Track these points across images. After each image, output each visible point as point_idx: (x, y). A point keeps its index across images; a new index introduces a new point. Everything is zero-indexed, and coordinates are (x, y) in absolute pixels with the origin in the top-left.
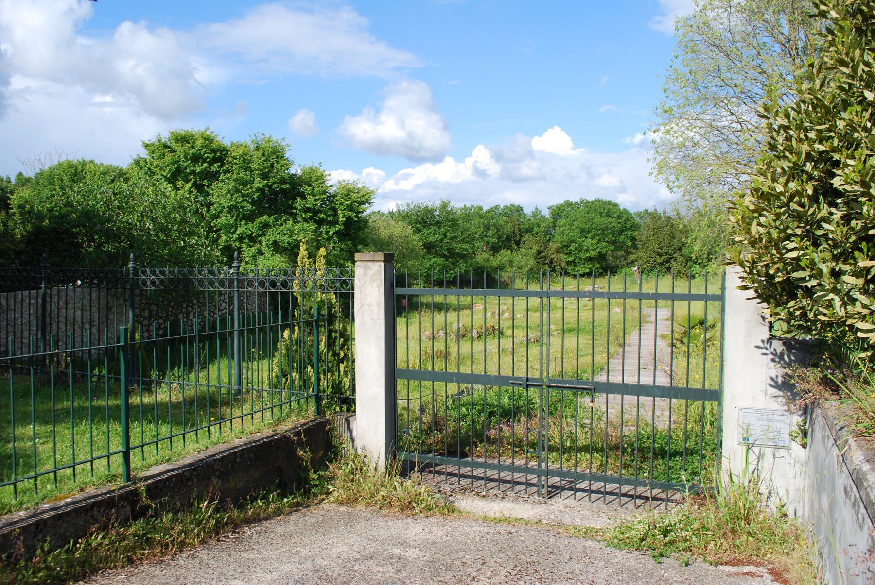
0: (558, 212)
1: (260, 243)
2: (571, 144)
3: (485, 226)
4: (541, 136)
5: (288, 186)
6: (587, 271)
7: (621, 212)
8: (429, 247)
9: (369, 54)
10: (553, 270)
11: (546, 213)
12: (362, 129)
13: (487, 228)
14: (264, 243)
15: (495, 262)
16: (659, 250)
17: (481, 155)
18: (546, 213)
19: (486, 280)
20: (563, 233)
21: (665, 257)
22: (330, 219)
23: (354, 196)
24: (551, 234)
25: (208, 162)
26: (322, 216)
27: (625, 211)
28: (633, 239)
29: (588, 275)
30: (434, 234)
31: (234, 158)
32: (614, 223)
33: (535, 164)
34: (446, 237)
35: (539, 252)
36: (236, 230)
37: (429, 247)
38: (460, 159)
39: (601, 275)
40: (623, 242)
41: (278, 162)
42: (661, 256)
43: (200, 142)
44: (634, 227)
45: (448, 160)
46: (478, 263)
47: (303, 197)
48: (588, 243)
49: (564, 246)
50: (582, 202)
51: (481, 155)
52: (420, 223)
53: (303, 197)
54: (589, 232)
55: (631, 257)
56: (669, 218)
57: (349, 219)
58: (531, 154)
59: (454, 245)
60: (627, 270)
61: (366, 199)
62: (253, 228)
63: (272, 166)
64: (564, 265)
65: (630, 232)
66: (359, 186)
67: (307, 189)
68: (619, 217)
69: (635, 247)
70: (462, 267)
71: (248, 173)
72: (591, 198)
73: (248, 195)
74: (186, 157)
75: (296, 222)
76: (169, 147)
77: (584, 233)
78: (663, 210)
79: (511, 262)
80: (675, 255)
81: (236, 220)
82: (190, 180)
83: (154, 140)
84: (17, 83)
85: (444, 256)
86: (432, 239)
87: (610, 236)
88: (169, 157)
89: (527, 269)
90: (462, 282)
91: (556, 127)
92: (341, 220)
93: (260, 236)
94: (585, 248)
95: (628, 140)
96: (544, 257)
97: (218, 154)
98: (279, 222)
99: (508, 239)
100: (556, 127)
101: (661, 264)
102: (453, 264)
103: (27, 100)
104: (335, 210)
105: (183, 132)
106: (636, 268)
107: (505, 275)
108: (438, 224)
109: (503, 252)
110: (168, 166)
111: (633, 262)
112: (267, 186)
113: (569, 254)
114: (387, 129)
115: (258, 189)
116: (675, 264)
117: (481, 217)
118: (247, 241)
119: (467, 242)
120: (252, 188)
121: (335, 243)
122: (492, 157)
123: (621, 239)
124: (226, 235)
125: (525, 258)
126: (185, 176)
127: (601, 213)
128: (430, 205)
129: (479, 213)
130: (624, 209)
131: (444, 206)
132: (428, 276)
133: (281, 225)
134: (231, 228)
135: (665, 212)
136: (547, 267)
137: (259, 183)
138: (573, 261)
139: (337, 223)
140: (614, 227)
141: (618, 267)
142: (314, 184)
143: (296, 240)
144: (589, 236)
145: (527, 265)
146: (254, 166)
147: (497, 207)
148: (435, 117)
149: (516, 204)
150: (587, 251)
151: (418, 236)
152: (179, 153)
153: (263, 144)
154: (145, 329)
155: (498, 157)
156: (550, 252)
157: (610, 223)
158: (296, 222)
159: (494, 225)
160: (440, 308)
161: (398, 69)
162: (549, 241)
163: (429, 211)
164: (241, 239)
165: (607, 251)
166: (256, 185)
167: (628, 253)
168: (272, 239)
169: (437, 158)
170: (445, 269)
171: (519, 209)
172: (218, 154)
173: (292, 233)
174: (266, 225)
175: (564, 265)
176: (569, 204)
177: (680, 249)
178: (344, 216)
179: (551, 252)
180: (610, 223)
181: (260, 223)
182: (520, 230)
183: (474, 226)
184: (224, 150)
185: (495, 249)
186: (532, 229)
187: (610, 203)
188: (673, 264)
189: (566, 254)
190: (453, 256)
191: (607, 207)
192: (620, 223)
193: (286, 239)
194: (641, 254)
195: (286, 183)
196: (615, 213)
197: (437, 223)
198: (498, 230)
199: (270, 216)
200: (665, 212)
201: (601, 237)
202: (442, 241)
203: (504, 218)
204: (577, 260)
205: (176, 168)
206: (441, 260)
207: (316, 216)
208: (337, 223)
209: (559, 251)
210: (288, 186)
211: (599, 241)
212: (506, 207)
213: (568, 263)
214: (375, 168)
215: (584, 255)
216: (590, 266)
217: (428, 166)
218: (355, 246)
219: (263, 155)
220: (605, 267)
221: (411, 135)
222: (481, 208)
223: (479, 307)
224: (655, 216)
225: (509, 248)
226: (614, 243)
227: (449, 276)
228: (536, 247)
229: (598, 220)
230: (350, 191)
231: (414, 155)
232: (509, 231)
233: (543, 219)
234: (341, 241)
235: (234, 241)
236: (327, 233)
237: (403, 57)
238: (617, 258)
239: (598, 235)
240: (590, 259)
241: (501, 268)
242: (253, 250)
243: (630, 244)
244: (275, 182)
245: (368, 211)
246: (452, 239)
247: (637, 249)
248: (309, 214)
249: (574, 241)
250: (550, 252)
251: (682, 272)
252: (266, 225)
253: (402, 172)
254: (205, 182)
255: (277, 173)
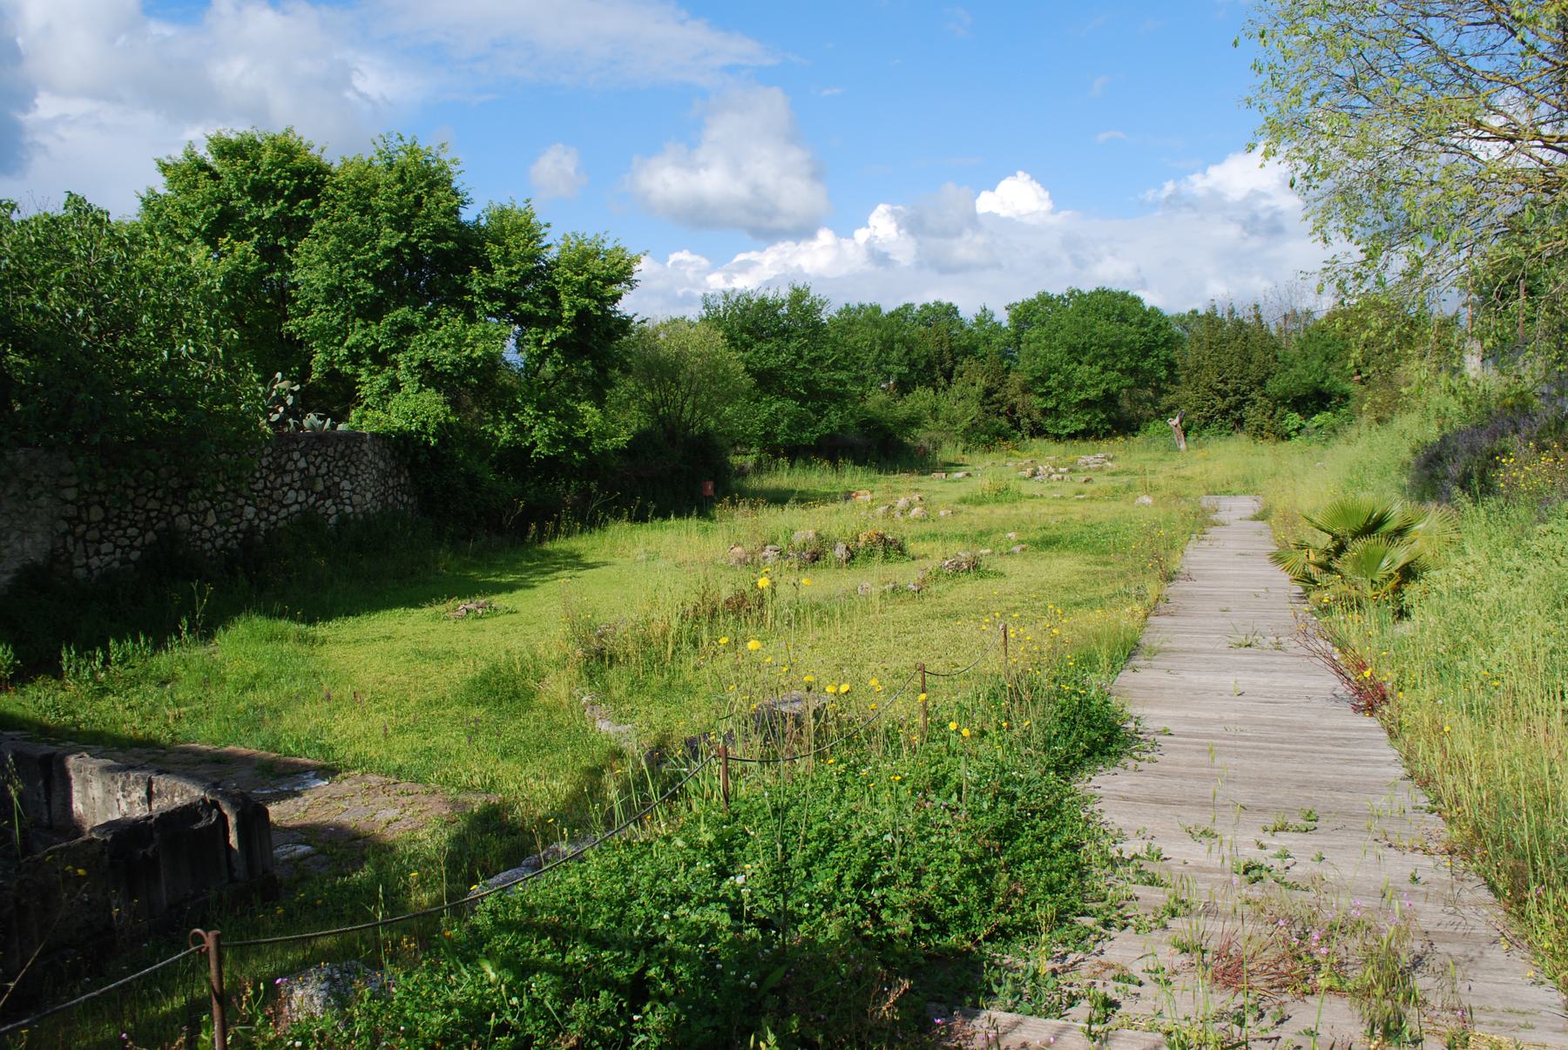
0: (1025, 315)
1: (395, 365)
2: (1047, 205)
3: (884, 343)
4: (993, 190)
5: (451, 244)
6: (1082, 426)
7: (1147, 314)
8: (767, 381)
9: (678, 44)
10: (1016, 425)
11: (1003, 318)
12: (667, 180)
13: (888, 345)
14: (402, 366)
15: (903, 409)
16: (1221, 386)
17: (882, 226)
18: (1003, 318)
19: (886, 449)
20: (1035, 354)
21: (1232, 399)
22: (543, 312)
23: (595, 265)
24: (1012, 358)
25: (287, 199)
26: (526, 306)
27: (1154, 312)
28: (1170, 365)
29: (1085, 435)
30: (778, 353)
31: (337, 187)
32: (1132, 334)
33: (979, 239)
34: (801, 357)
35: (989, 393)
36: (345, 339)
37: (767, 381)
38: (844, 230)
39: (1108, 434)
40: (1151, 371)
41: (430, 195)
42: (1224, 396)
43: (266, 157)
44: (1171, 342)
45: (825, 236)
46: (867, 412)
47: (487, 268)
48: (1082, 372)
49: (1036, 379)
50: (1071, 294)
51: (882, 226)
52: (750, 332)
53: (487, 268)
54: (1084, 351)
55: (1166, 401)
56: (1240, 325)
57: (583, 314)
58: (973, 221)
59: (818, 373)
60: (1159, 424)
61: (622, 275)
62: (379, 333)
63: (418, 202)
64: (1036, 416)
65: (1164, 351)
66: (608, 246)
67: (494, 250)
68: (1142, 324)
69: (1173, 379)
70: (833, 418)
71: (366, 218)
72: (1087, 288)
73: (365, 264)
74: (239, 188)
75: (471, 319)
76: (209, 169)
77: (1075, 353)
78: (1227, 307)
79: (935, 411)
80: (1253, 395)
81: (345, 318)
82: (252, 236)
83: (178, 155)
84: (46, 107)
85: (798, 396)
86: (772, 362)
87: (1127, 359)
88: (206, 186)
89: (965, 423)
90: (833, 450)
91: (1020, 174)
92: (566, 314)
93: (394, 350)
94: (1077, 382)
95: (1150, 195)
96: (998, 401)
97: (307, 181)
98: (435, 322)
99: (930, 366)
100: (1020, 174)
101: (1225, 413)
102: (816, 411)
103: (62, 139)
104: (554, 295)
105: (233, 137)
106: (1177, 421)
107: (921, 437)
108: (785, 333)
109: (919, 391)
110: (203, 206)
111: (1170, 409)
112: (405, 243)
113: (1047, 394)
114: (713, 181)
115: (387, 252)
116: (1252, 412)
117: (876, 324)
118: (368, 361)
119: (844, 368)
120: (373, 249)
121: (556, 364)
122: (899, 227)
123: (1147, 364)
124: (324, 350)
125: (962, 403)
126: (240, 229)
127: (1108, 316)
128: (770, 295)
129: (872, 316)
130: (1152, 308)
131: (798, 296)
132: (768, 436)
133: (437, 327)
134: (334, 336)
135: (1232, 312)
136: (1002, 426)
137: (389, 238)
138: (1055, 409)
139: (559, 321)
140: (1133, 341)
141: (1140, 418)
142: (510, 241)
143: (468, 358)
144: (1085, 359)
145: (965, 415)
146: (378, 202)
147: (908, 307)
148: (795, 156)
149: (945, 301)
150: (1081, 388)
151: (735, 355)
152: (226, 181)
153: (401, 158)
154: (91, 551)
155: (914, 225)
156: (1011, 391)
157: (1127, 333)
158: (471, 319)
159: (902, 340)
160: (779, 498)
161: (731, 70)
162: (1007, 370)
163: (766, 308)
164: (355, 358)
165: (1120, 389)
166: (383, 242)
167: (1160, 392)
168: (419, 355)
169: (804, 232)
170: (799, 424)
171: (951, 311)
172: (307, 181)
173: (460, 341)
174: (407, 329)
175: (1036, 416)
176: (1045, 300)
177: (1262, 383)
178: (573, 306)
179: (1012, 391)
180: (1127, 333)
181: (394, 323)
182: (951, 350)
183: (861, 338)
184: (319, 173)
185: (904, 387)
186: (976, 348)
187: (1124, 295)
188: (1249, 412)
189: (1041, 395)
190: (814, 395)
191: (1120, 304)
192: (1144, 334)
193: (448, 355)
194: (1185, 392)
195: (447, 238)
196: (1135, 315)
197: (785, 330)
198: (910, 350)
199: (415, 309)
200: (1232, 312)
201: (1109, 361)
202: (793, 366)
203: (922, 328)
204: (1062, 407)
205: (221, 213)
206: (791, 405)
207: (514, 307)
208: (559, 321)
209: (1026, 389)
210: (451, 244)
211: (1105, 369)
212: (926, 307)
213: (1045, 412)
214: (693, 253)
215: (1075, 397)
216: (1087, 418)
217: (787, 247)
218: (602, 371)
219: (401, 180)
220: (1114, 420)
221: (755, 188)
222: (877, 310)
223: (864, 497)
224: (1211, 320)
225: (932, 383)
226: (1133, 371)
227: (808, 437)
228: (982, 382)
229: (1102, 327)
230: (586, 256)
231: (765, 225)
232: (929, 350)
233: (997, 328)
234: (569, 359)
235: (342, 363)
236: (539, 342)
237: (739, 48)
238: (1140, 402)
239: (1103, 357)
240: (1087, 404)
241: (913, 422)
242: (381, 381)
243: (1163, 374)
244: (423, 237)
245: (628, 305)
246: (813, 362)
247: (1178, 384)
248: (499, 304)
249: (1056, 370)
250: (1011, 391)
251: (1267, 426)
252: (407, 329)
253: (741, 257)
254: (283, 241)
255: (427, 216)
